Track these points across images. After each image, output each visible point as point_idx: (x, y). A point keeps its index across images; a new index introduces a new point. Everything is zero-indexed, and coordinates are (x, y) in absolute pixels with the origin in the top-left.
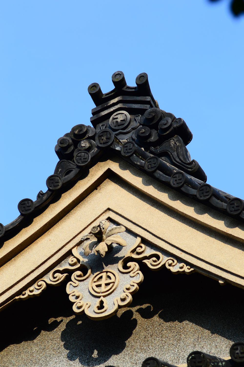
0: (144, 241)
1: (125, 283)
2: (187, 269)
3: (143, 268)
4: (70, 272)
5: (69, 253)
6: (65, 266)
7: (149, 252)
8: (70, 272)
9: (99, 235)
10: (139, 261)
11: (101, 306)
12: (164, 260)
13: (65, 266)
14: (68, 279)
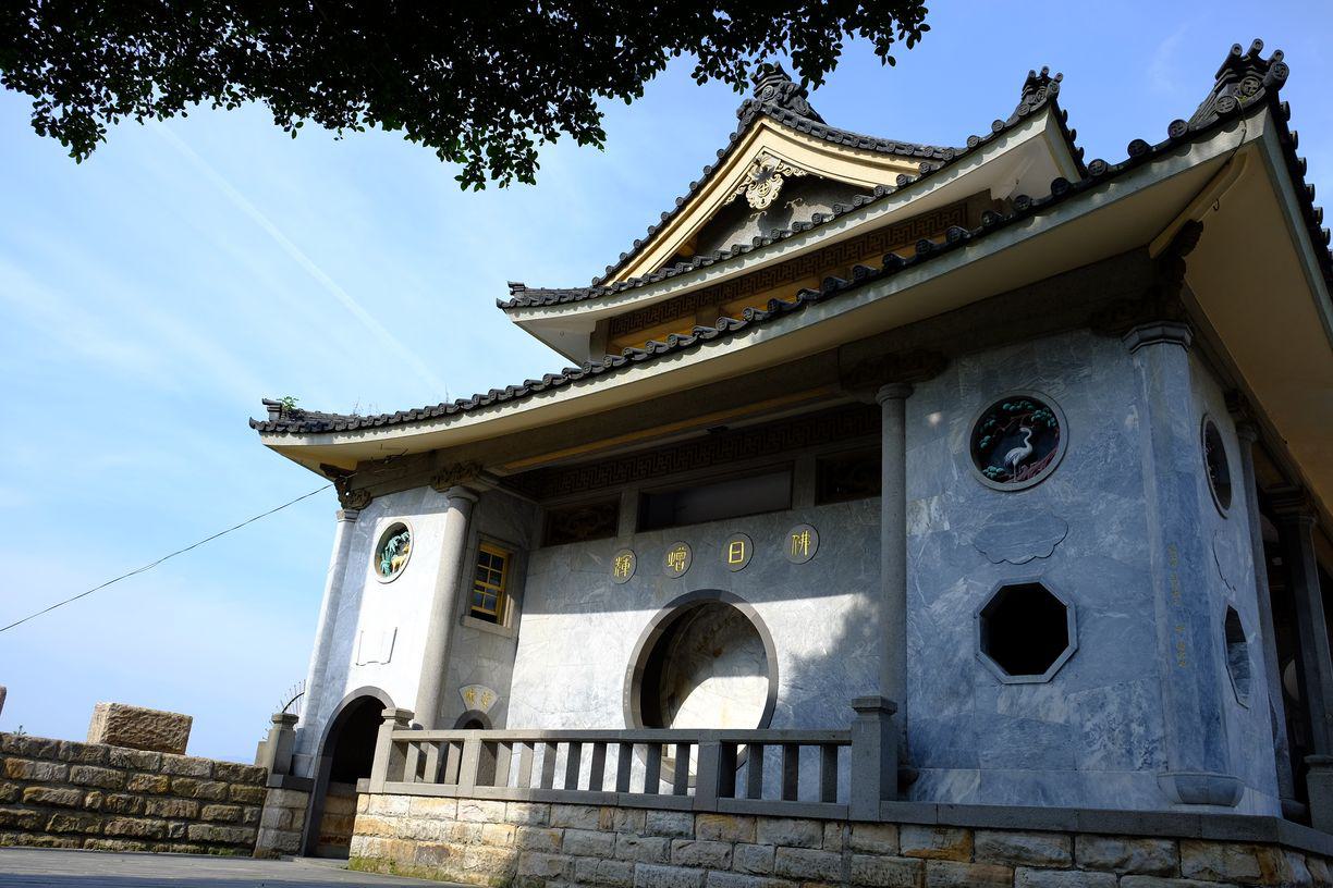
0: (782, 161)
1: (775, 185)
2: (804, 174)
3: (783, 177)
4: (747, 186)
5: (746, 175)
6: (745, 183)
7: (786, 166)
8: (747, 186)
9: (758, 162)
10: (780, 173)
11: (763, 202)
12: (793, 170)
13: (745, 183)
14: (746, 190)
